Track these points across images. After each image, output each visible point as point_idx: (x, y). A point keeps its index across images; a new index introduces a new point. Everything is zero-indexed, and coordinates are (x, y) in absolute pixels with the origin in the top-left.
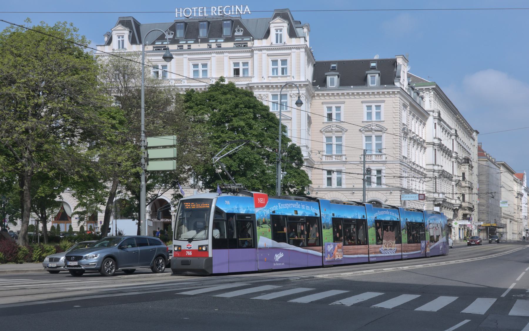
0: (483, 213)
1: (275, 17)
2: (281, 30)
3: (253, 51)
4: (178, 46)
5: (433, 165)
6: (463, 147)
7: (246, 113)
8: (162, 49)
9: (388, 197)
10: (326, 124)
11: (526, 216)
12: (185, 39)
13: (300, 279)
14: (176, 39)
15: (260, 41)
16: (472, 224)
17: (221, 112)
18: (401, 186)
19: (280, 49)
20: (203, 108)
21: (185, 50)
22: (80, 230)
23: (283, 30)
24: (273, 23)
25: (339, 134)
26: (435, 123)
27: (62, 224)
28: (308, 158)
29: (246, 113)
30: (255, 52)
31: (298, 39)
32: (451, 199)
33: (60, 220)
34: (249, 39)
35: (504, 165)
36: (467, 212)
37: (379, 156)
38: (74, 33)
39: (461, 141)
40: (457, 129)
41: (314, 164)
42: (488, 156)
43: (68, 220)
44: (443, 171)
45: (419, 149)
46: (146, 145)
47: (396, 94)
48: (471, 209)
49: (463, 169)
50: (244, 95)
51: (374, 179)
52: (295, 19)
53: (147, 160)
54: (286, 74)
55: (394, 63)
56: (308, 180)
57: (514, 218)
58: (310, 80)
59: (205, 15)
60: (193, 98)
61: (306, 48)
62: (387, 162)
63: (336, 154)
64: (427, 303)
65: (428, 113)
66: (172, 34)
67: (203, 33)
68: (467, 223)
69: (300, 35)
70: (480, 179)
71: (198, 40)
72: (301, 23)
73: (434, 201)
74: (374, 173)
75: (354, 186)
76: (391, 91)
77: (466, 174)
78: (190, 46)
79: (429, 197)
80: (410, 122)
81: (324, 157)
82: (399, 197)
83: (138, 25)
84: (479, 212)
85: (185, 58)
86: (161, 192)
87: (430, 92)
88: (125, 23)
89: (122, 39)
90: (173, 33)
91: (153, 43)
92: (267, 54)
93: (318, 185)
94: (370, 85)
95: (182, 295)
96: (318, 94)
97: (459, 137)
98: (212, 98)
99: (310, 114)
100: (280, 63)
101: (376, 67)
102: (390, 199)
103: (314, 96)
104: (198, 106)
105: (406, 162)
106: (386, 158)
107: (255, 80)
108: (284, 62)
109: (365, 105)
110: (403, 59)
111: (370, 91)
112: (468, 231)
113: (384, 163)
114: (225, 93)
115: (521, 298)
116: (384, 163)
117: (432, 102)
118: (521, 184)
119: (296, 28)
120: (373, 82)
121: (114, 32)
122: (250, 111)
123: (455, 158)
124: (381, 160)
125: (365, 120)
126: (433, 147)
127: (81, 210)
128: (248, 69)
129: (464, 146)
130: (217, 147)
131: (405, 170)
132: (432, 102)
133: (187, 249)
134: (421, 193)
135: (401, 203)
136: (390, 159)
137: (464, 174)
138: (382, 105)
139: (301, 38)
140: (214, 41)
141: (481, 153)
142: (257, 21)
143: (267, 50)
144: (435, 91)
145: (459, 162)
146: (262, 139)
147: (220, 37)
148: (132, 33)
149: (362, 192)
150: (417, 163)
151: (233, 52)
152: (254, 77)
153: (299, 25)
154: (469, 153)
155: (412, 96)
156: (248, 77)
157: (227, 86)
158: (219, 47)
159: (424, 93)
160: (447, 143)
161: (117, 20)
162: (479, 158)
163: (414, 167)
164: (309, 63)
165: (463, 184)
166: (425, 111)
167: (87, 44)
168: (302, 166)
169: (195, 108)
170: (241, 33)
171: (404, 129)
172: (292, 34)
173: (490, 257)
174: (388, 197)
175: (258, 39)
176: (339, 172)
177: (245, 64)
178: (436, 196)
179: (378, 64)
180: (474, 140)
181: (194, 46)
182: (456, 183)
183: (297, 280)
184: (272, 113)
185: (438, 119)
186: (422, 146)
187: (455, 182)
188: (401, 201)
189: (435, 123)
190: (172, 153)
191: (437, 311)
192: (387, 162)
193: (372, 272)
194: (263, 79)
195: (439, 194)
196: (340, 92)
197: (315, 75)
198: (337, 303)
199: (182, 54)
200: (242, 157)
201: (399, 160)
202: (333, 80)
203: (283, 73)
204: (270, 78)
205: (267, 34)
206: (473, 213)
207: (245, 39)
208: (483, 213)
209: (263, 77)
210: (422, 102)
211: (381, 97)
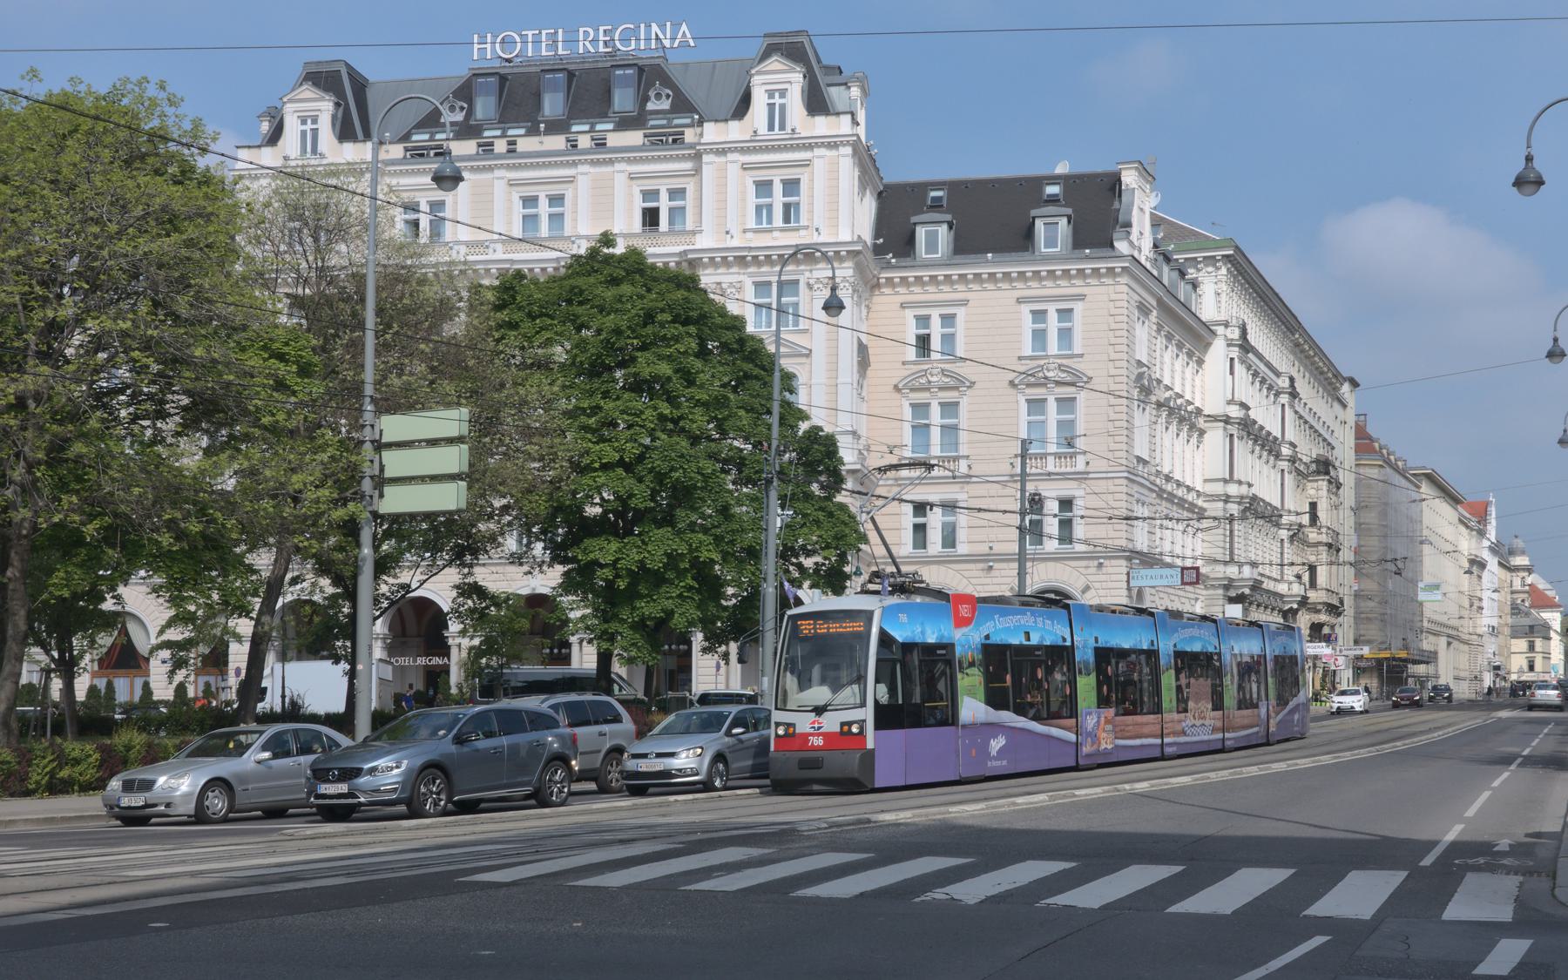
1: (765, 56)
2: (783, 93)
4: (479, 145)
6: (1311, 427)
7: (677, 339)
10: (912, 366)
11: (1493, 627)
12: (499, 122)
13: (830, 827)
14: (472, 122)
15: (721, 125)
16: (1338, 653)
19: (779, 149)
20: (550, 325)
21: (500, 157)
22: (175, 696)
23: (788, 94)
24: (759, 73)
26: (1232, 359)
27: (122, 679)
28: (858, 467)
30: (705, 158)
31: (832, 119)
32: (1275, 580)
34: (688, 121)
35: (1431, 478)
36: (1323, 618)
37: (1065, 458)
38: (170, 111)
39: (1307, 410)
40: (1295, 375)
42: (1385, 451)
43: (139, 667)
44: (1254, 498)
46: (378, 438)
47: (1119, 275)
49: (1312, 492)
51: (1051, 526)
52: (825, 62)
54: (797, 220)
55: (1112, 185)
57: (1460, 634)
58: (868, 237)
60: (519, 298)
61: (856, 146)
63: (939, 454)
66: (462, 108)
67: (553, 104)
70: (1362, 521)
71: (539, 127)
72: (841, 72)
73: (1227, 588)
74: (1052, 506)
75: (991, 548)
77: (1319, 507)
78: (514, 143)
79: (1212, 576)
80: (1158, 357)
82: (1125, 578)
83: (360, 85)
84: (1358, 618)
85: (498, 178)
86: (419, 577)
87: (1218, 269)
88: (323, 79)
89: (314, 127)
90: (466, 106)
91: (406, 138)
94: (1043, 250)
95: (477, 883)
96: (889, 280)
97: (1301, 399)
98: (575, 296)
99: (864, 339)
100: (778, 188)
101: (1061, 197)
102: (1097, 585)
103: (878, 286)
105: (1146, 475)
106: (1088, 463)
107: (704, 241)
108: (791, 186)
109: (1026, 309)
110: (1140, 173)
111: (1044, 268)
112: (1325, 672)
113: (1081, 477)
114: (614, 281)
115: (1477, 869)
116: (1081, 477)
117: (1223, 296)
118: (1482, 533)
120: (1051, 242)
121: (288, 105)
122: (688, 333)
123: (1289, 461)
124: (1073, 470)
125: (1028, 352)
126: (1225, 429)
127: (179, 638)
128: (683, 208)
129: (1315, 424)
130: (590, 440)
131: (1143, 498)
132: (1224, 297)
133: (812, 731)
134: (1189, 563)
135: (1130, 597)
136: (1098, 465)
137: (1313, 506)
138: (1078, 307)
139: (841, 116)
140: (586, 128)
141: (1364, 443)
142: (714, 67)
143: (743, 151)
144: (1233, 265)
145: (1299, 472)
146: (721, 413)
147: (603, 115)
148: (342, 108)
149: (1016, 565)
150: (1177, 476)
152: (701, 232)
153: (837, 79)
154: (1329, 444)
156: (684, 232)
157: (621, 259)
158: (600, 144)
160: (1267, 416)
161: (298, 71)
162: (1360, 460)
163: (1169, 487)
165: (1311, 535)
166: (1204, 323)
167: (209, 141)
168: (838, 491)
169: (527, 327)
170: (665, 105)
171: (1140, 376)
172: (817, 104)
173: (1388, 748)
174: (1091, 578)
175: (716, 121)
176: (950, 506)
178: (1232, 571)
179: (1066, 190)
180: (1344, 406)
181: (526, 144)
182: (1291, 533)
183: (819, 829)
184: (752, 338)
185: (1241, 346)
186: (1192, 427)
187: (1289, 530)
188: (1129, 589)
189: (1232, 359)
190: (453, 459)
191: (1234, 913)
192: (1091, 476)
194: (729, 236)
195: (1240, 565)
196: (955, 272)
197: (881, 226)
198: (939, 894)
199: (490, 169)
200: (665, 467)
201: (1124, 468)
202: (933, 237)
203: (787, 219)
204: (749, 235)
205: (743, 106)
207: (677, 122)
208: (1369, 619)
209: (727, 233)
210: (1194, 297)
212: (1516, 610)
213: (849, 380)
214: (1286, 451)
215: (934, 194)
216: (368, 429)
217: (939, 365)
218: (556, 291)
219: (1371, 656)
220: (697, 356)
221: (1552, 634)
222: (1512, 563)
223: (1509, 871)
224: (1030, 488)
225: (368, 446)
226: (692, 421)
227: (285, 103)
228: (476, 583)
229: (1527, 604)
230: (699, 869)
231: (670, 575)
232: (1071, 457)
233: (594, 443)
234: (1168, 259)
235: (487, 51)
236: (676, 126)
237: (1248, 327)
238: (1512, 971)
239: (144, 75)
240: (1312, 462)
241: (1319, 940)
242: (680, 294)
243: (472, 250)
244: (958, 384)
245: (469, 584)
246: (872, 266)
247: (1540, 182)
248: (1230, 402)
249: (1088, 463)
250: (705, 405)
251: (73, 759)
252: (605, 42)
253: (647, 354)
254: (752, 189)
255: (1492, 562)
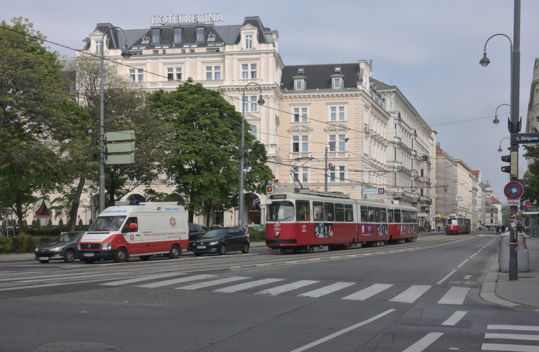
0: (441, 206)
2: (251, 36)
3: (225, 56)
5: (393, 162)
7: (212, 112)
8: (139, 53)
9: (350, 191)
10: (293, 124)
11: (480, 209)
12: (160, 44)
13: (241, 268)
14: (151, 44)
15: (231, 46)
17: (187, 111)
18: (362, 181)
19: (250, 54)
21: (160, 55)
22: (59, 224)
23: (253, 36)
24: (243, 29)
25: (305, 134)
26: (396, 124)
27: (43, 218)
28: (276, 155)
29: (212, 112)
30: (226, 57)
31: (266, 45)
32: (410, 193)
33: (41, 215)
34: (221, 45)
36: (425, 205)
37: (342, 153)
38: (29, 28)
39: (420, 141)
41: (282, 161)
42: (446, 154)
43: (49, 215)
44: (403, 167)
45: (380, 147)
48: (429, 203)
50: (210, 95)
52: (265, 26)
53: (106, 154)
54: (256, 77)
55: (356, 68)
56: (271, 174)
57: (469, 211)
59: (180, 22)
60: (161, 98)
61: (274, 53)
62: (350, 159)
64: (358, 291)
65: (389, 115)
66: (148, 39)
67: (177, 38)
68: (425, 215)
69: (270, 41)
72: (270, 30)
73: (394, 195)
75: (318, 181)
76: (353, 93)
80: (372, 123)
81: (291, 155)
82: (361, 191)
84: (437, 205)
86: (132, 187)
87: (391, 95)
88: (103, 28)
90: (149, 38)
92: (237, 59)
93: (285, 181)
95: (104, 286)
96: (286, 97)
97: (418, 137)
98: (180, 98)
100: (249, 67)
103: (282, 98)
104: (166, 105)
105: (367, 159)
106: (349, 155)
107: (227, 83)
108: (254, 66)
109: (329, 107)
110: (365, 64)
111: (335, 94)
114: (192, 93)
115: (456, 285)
118: (476, 181)
119: (266, 34)
120: (337, 85)
121: (92, 37)
123: (414, 156)
124: (344, 157)
125: (330, 120)
126: (393, 146)
127: (58, 205)
128: (219, 73)
130: (184, 144)
131: (366, 167)
134: (382, 187)
135: (362, 197)
136: (352, 156)
137: (422, 171)
138: (346, 106)
139: (270, 44)
140: (188, 46)
143: (238, 54)
144: (396, 94)
146: (227, 136)
149: (324, 187)
150: (378, 160)
151: (206, 57)
152: (225, 80)
154: (427, 151)
155: (374, 99)
156: (219, 80)
157: (195, 86)
158: (192, 52)
159: (385, 96)
160: (407, 142)
161: (95, 26)
163: (375, 163)
164: (278, 67)
166: (387, 112)
168: (266, 162)
169: (164, 107)
171: (365, 128)
172: (262, 39)
173: (440, 245)
174: (350, 191)
175: (230, 45)
177: (217, 68)
178: (396, 190)
179: (342, 69)
180: (433, 140)
181: (169, 51)
182: (415, 179)
184: (238, 113)
185: (398, 120)
186: (383, 145)
188: (362, 195)
189: (396, 124)
190: (130, 147)
191: (365, 300)
192: (350, 159)
193: (318, 260)
196: (306, 94)
197: (283, 79)
198: (264, 292)
199: (157, 59)
200: (208, 153)
201: (360, 157)
202: (300, 83)
203: (253, 77)
204: (241, 81)
205: (238, 41)
206: (431, 206)
208: (441, 206)
209: (233, 81)
210: (383, 104)
211: (344, 99)
212: (487, 204)
213: (273, 128)
214: (413, 153)
215: (300, 70)
216: (102, 137)
217: (302, 124)
218: (174, 96)
219: (441, 217)
220: (220, 118)
221: (499, 212)
222: (486, 190)
223: (467, 286)
224: (329, 162)
225: (102, 144)
226: (217, 138)
227: (91, 36)
228: (151, 189)
229: (491, 202)
230: (186, 282)
231: (211, 187)
232: (344, 153)
233: (185, 145)
234: (375, 92)
235: (157, 23)
236: (217, 46)
237: (401, 114)
238: (456, 324)
239: (20, 16)
240: (422, 157)
241: (391, 310)
242: (213, 98)
243: (152, 85)
244: (307, 130)
245: (149, 190)
246: (280, 92)
247: (488, 62)
248: (395, 137)
249: (349, 155)
250: (222, 134)
251: (3, 242)
252: (194, 19)
253: (203, 117)
254: (241, 67)
255: (480, 190)
